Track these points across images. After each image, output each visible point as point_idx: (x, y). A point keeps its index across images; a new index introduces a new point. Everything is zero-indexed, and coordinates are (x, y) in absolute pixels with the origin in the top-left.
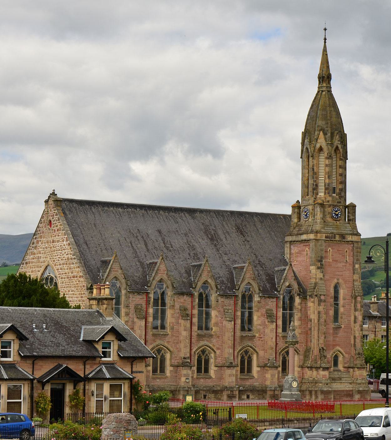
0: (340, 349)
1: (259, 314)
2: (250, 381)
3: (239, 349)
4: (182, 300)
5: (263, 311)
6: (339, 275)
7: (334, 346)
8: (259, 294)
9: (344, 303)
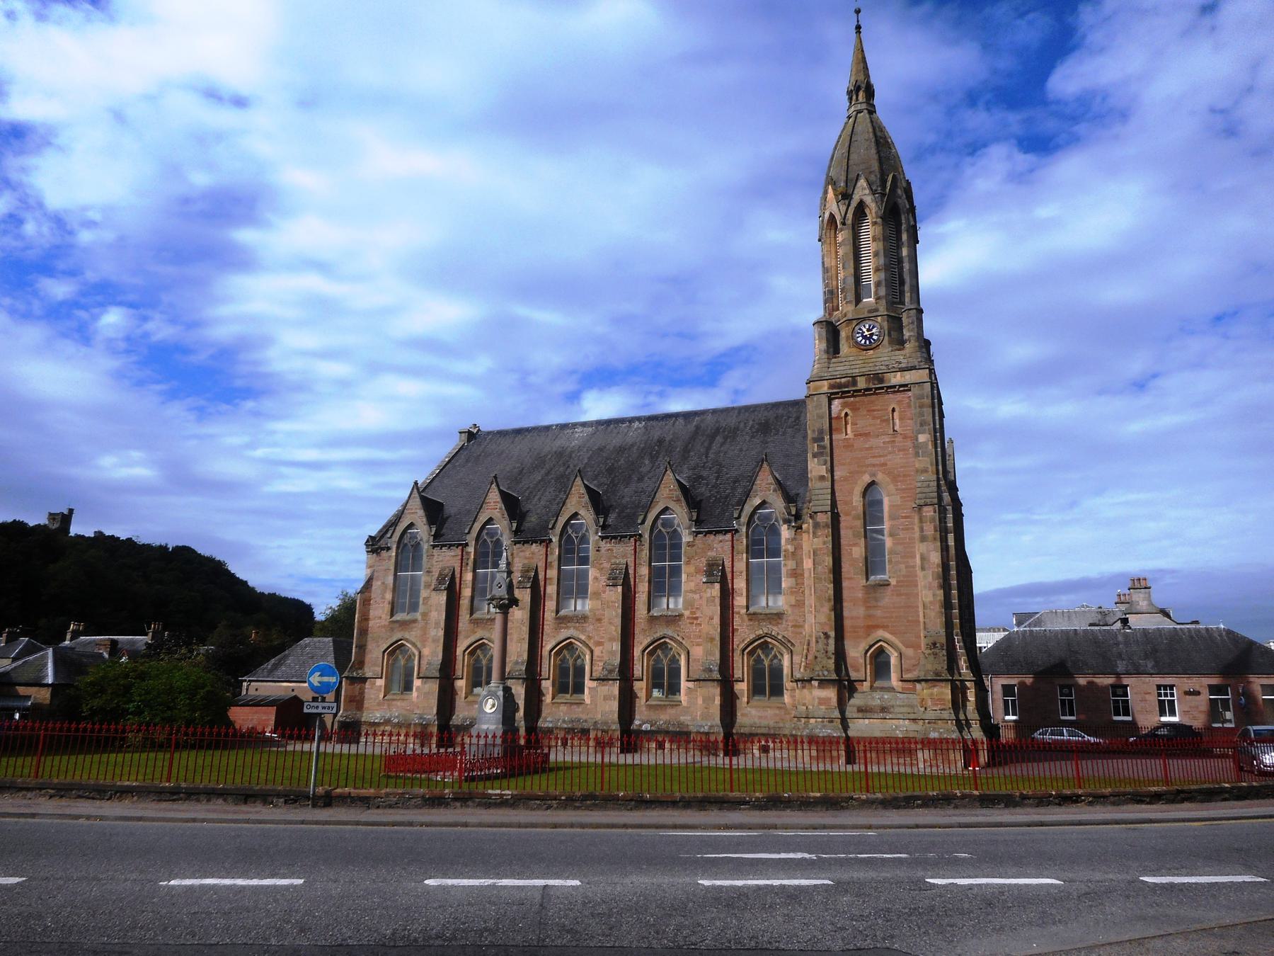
0: (887, 636)
1: (692, 569)
2: (672, 711)
3: (646, 642)
4: (527, 554)
5: (702, 563)
6: (874, 465)
7: (870, 628)
8: (690, 528)
9: (892, 527)
